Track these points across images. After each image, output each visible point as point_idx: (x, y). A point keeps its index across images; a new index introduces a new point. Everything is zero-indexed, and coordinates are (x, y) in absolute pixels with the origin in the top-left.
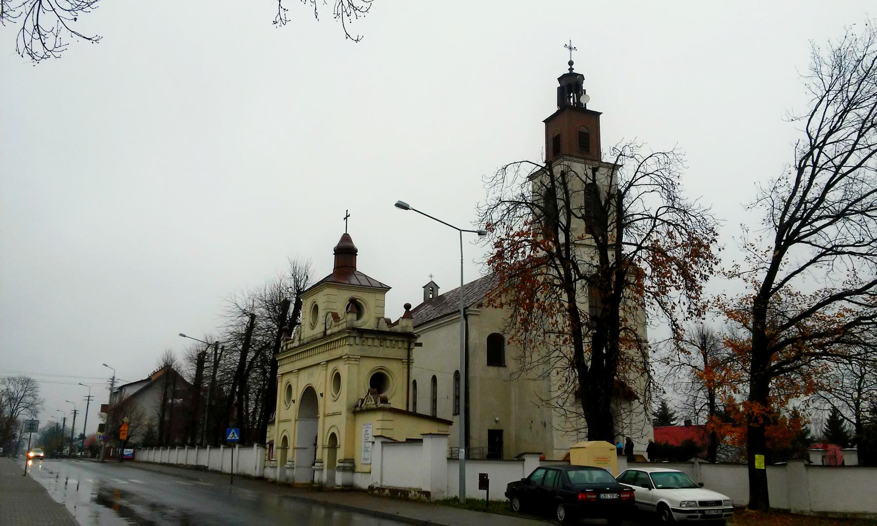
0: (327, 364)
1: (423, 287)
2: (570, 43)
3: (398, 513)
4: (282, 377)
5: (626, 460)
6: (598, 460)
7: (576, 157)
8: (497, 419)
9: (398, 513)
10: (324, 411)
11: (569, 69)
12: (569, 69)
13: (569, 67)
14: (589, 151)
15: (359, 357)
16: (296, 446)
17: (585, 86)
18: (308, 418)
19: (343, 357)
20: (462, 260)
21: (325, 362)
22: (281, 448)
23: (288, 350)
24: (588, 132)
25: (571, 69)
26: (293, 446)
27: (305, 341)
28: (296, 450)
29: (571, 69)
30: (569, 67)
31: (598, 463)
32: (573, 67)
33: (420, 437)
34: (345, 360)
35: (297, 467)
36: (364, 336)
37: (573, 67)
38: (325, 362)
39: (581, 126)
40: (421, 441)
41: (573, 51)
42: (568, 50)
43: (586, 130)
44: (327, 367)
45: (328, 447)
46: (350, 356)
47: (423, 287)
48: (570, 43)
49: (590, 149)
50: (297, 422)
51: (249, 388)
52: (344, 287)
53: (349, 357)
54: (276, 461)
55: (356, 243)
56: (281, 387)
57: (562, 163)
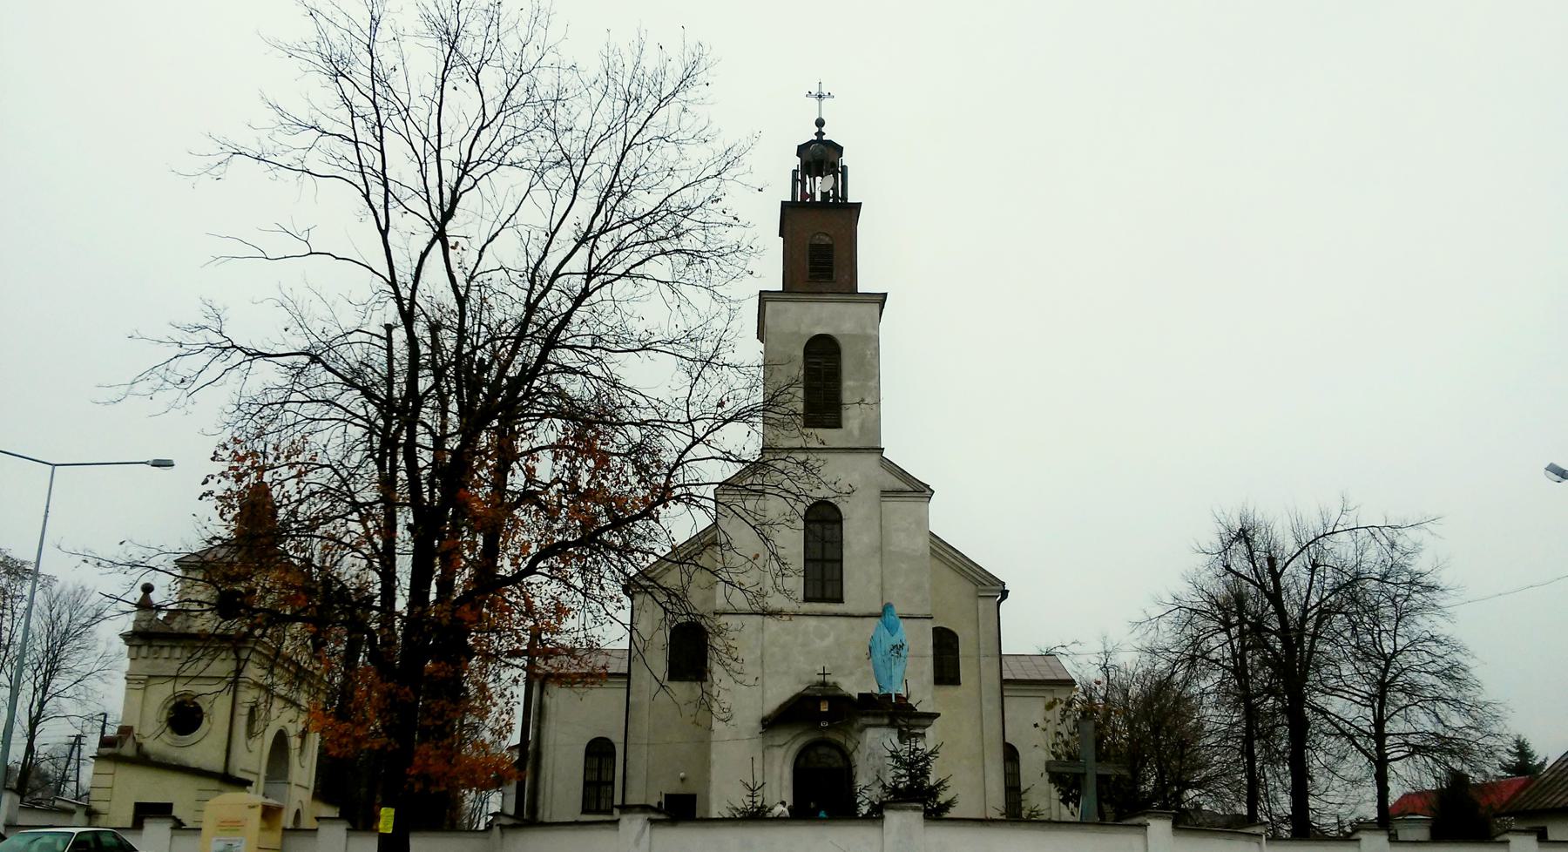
2: (820, 87)
5: (1536, 838)
6: (223, 824)
7: (809, 293)
8: (682, 774)
11: (816, 134)
12: (816, 134)
13: (817, 130)
14: (830, 277)
17: (846, 159)
20: (48, 507)
24: (831, 242)
25: (820, 134)
29: (820, 134)
30: (817, 130)
31: (221, 830)
32: (823, 130)
33: (315, 825)
36: (155, 644)
37: (823, 130)
39: (815, 235)
40: (317, 830)
41: (825, 102)
42: (815, 101)
43: (827, 239)
48: (820, 87)
49: (835, 272)
51: (1206, 776)
55: (220, 472)
56: (313, 757)
57: (560, 318)
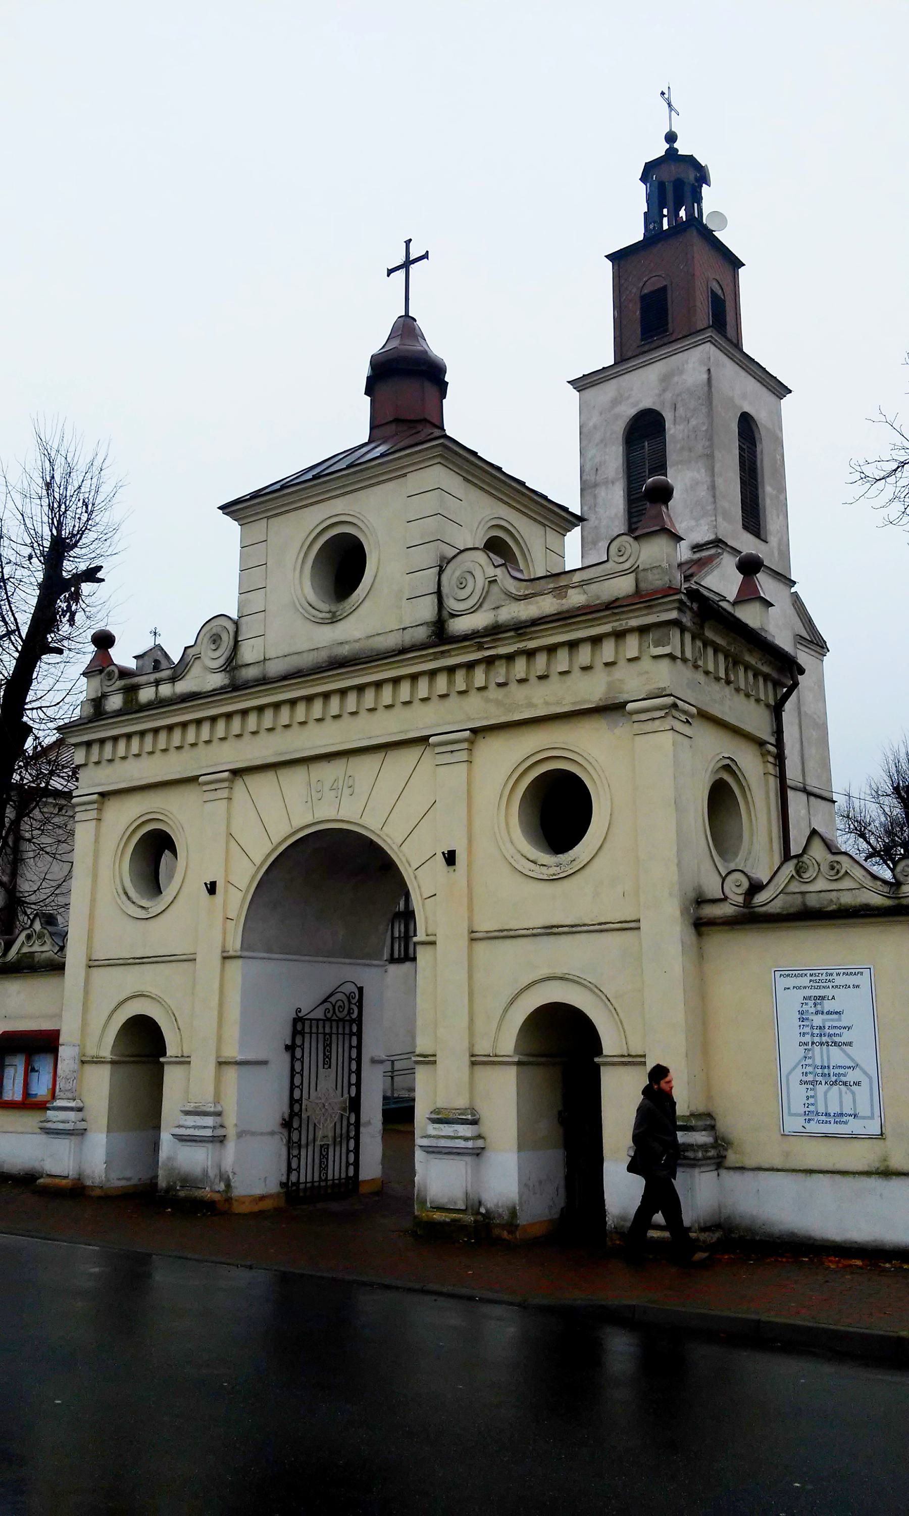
0: (472, 742)
1: (135, 657)
3: (435, 1300)
4: (103, 803)
9: (435, 1300)
10: (90, 947)
15: (694, 710)
16: (232, 1052)
18: (269, 950)
19: (201, 779)
21: (226, 774)
22: (112, 1062)
23: (159, 704)
26: (218, 1057)
27: (250, 673)
28: (231, 1074)
34: (205, 788)
35: (240, 1135)
38: (226, 774)
44: (100, 810)
45: (519, 1064)
46: (679, 703)
47: (135, 657)
50: (235, 967)
52: (478, 473)
53: (675, 706)
54: (80, 1110)
